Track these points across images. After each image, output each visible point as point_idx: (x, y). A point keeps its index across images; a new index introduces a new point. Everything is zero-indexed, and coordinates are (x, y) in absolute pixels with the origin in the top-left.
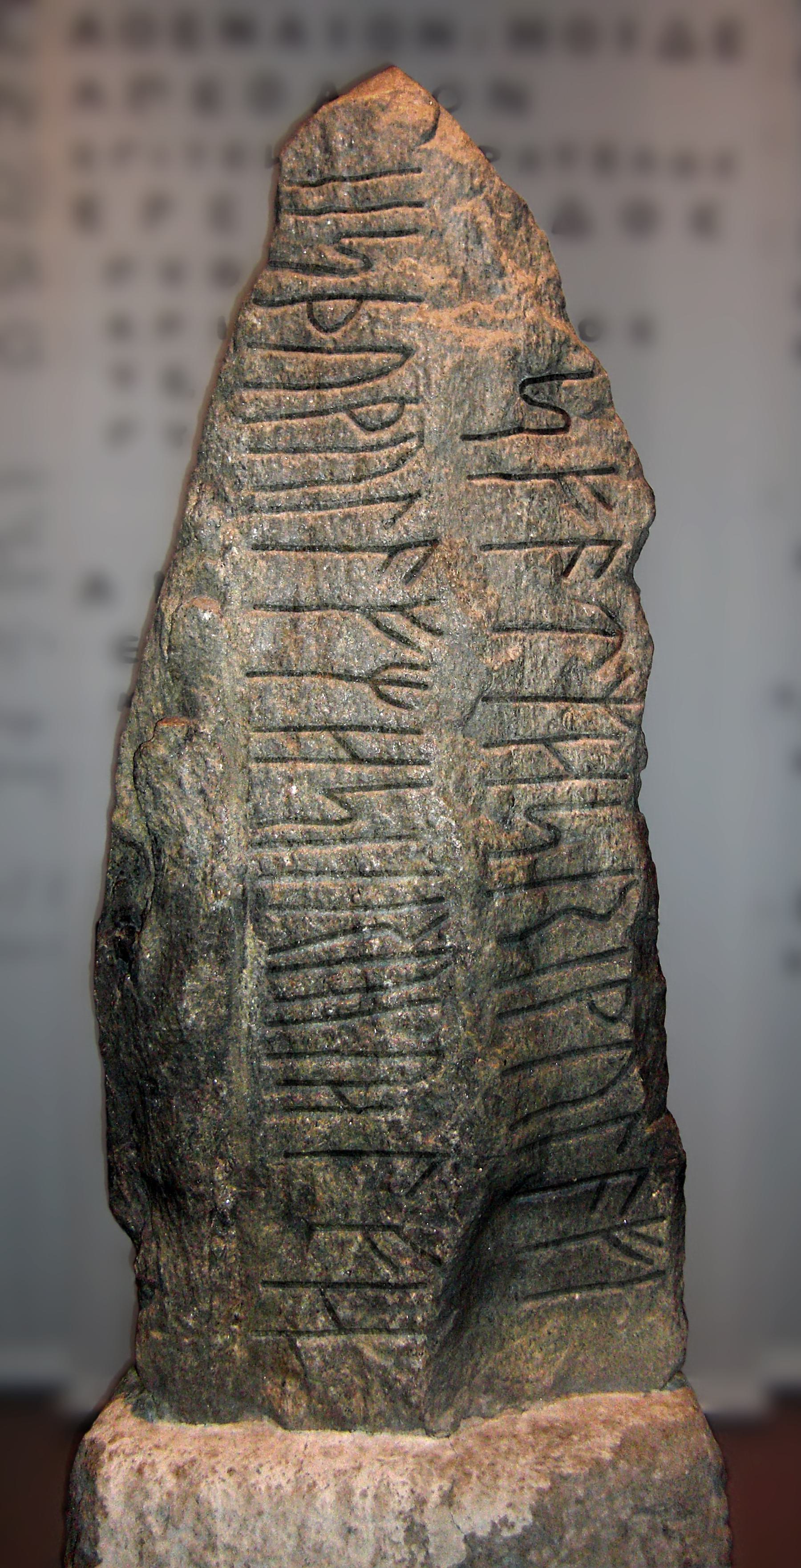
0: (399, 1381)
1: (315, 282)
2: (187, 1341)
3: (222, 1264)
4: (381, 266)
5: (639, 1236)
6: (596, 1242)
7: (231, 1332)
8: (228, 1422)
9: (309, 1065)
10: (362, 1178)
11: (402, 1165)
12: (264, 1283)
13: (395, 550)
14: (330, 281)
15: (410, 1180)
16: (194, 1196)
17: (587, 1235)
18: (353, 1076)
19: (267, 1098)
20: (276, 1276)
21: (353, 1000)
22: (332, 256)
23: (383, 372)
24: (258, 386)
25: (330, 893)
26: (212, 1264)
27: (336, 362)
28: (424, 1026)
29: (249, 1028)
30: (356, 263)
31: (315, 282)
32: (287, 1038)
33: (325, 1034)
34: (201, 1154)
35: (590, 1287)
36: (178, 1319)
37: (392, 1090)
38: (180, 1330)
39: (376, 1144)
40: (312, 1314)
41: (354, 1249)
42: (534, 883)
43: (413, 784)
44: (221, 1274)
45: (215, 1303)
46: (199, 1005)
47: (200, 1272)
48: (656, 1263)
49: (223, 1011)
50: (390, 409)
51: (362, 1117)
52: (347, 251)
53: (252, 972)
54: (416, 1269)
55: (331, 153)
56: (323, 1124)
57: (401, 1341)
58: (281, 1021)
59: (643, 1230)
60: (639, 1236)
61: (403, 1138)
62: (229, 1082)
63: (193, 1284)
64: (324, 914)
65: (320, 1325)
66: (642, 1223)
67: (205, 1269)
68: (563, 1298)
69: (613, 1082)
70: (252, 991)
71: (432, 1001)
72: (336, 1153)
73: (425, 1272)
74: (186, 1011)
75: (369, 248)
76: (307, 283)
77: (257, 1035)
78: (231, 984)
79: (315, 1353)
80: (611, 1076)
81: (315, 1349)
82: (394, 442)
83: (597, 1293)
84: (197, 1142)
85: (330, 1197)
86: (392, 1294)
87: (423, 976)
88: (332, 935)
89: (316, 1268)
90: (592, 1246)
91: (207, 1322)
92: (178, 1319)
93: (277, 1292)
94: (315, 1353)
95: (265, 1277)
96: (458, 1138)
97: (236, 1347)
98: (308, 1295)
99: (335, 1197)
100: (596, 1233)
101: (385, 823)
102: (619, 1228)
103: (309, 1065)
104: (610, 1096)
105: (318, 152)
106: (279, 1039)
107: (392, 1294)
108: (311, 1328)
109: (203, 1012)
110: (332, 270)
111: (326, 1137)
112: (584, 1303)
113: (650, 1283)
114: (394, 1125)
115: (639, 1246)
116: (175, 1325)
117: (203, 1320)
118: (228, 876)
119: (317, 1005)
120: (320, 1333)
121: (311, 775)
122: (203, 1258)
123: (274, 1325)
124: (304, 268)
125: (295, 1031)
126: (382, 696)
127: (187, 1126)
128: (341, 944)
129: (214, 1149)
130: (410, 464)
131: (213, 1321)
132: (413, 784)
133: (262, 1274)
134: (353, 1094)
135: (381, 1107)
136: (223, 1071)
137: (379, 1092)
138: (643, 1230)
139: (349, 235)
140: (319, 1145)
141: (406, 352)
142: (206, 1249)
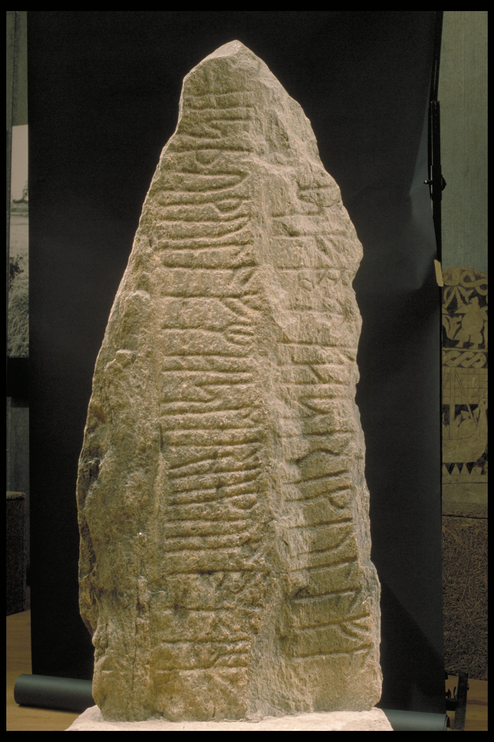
0: (233, 692)
1: (199, 141)
2: (122, 673)
3: (142, 632)
4: (231, 136)
5: (357, 625)
6: (334, 627)
7: (145, 669)
8: (142, 721)
9: (188, 525)
10: (214, 585)
11: (235, 576)
12: (164, 641)
13: (236, 268)
14: (207, 141)
15: (240, 584)
16: (128, 596)
17: (330, 623)
18: (211, 530)
19: (167, 543)
20: (171, 637)
21: (213, 491)
22: (208, 129)
23: (231, 184)
24: (172, 189)
25: (203, 436)
26: (137, 632)
27: (209, 180)
28: (250, 505)
29: (159, 507)
30: (218, 132)
31: (199, 141)
32: (177, 512)
33: (198, 508)
34: (133, 573)
35: (331, 653)
36: (118, 662)
37: (230, 537)
38: (119, 667)
39: (222, 565)
40: (188, 657)
41: (210, 621)
42: (305, 435)
43: (245, 381)
44: (141, 637)
45: (137, 653)
46: (134, 494)
47: (130, 635)
48: (365, 639)
49: (146, 497)
50: (234, 202)
51: (216, 552)
52: (215, 127)
53: (162, 477)
54: (242, 631)
55: (208, 82)
56: (196, 556)
57: (233, 670)
58: (174, 503)
59: (358, 621)
60: (357, 625)
61: (238, 562)
62: (148, 535)
63: (126, 642)
64: (199, 448)
65: (192, 664)
66: (358, 618)
67: (133, 634)
68: (317, 657)
69: (342, 541)
70: (162, 488)
71: (252, 492)
72: (202, 572)
73: (247, 633)
74: (127, 497)
75: (226, 126)
76: (195, 142)
77: (163, 511)
78: (152, 483)
79: (189, 678)
80: (341, 537)
81: (189, 676)
82: (237, 217)
83: (334, 656)
84: (130, 566)
85: (199, 594)
86: (229, 645)
87: (247, 479)
88: (202, 459)
89: (190, 632)
90: (332, 629)
91: (133, 664)
92: (118, 662)
93: (169, 645)
94: (189, 678)
95: (164, 638)
96: (264, 562)
97: (148, 678)
98: (185, 646)
99: (201, 594)
100: (334, 623)
101: (230, 401)
102: (345, 620)
103: (188, 525)
104: (341, 548)
105: (202, 81)
106: (174, 512)
107: (229, 645)
108: (187, 664)
109: (136, 498)
110: (207, 135)
111: (198, 562)
112: (328, 662)
113: (362, 651)
114: (231, 556)
115: (356, 630)
116: (116, 665)
117: (131, 662)
118: (151, 428)
119: (194, 494)
120: (192, 668)
121: (192, 378)
122: (132, 628)
123: (168, 665)
124: (193, 134)
125: (183, 508)
126: (231, 340)
127: (126, 558)
128: (207, 463)
129: (139, 571)
130: (245, 229)
131: (136, 662)
132: (245, 381)
133: (162, 636)
134: (212, 539)
135: (225, 546)
136: (144, 529)
137: (224, 539)
138: (358, 621)
139: (216, 119)
140: (194, 566)
141: (242, 174)
142: (134, 623)
